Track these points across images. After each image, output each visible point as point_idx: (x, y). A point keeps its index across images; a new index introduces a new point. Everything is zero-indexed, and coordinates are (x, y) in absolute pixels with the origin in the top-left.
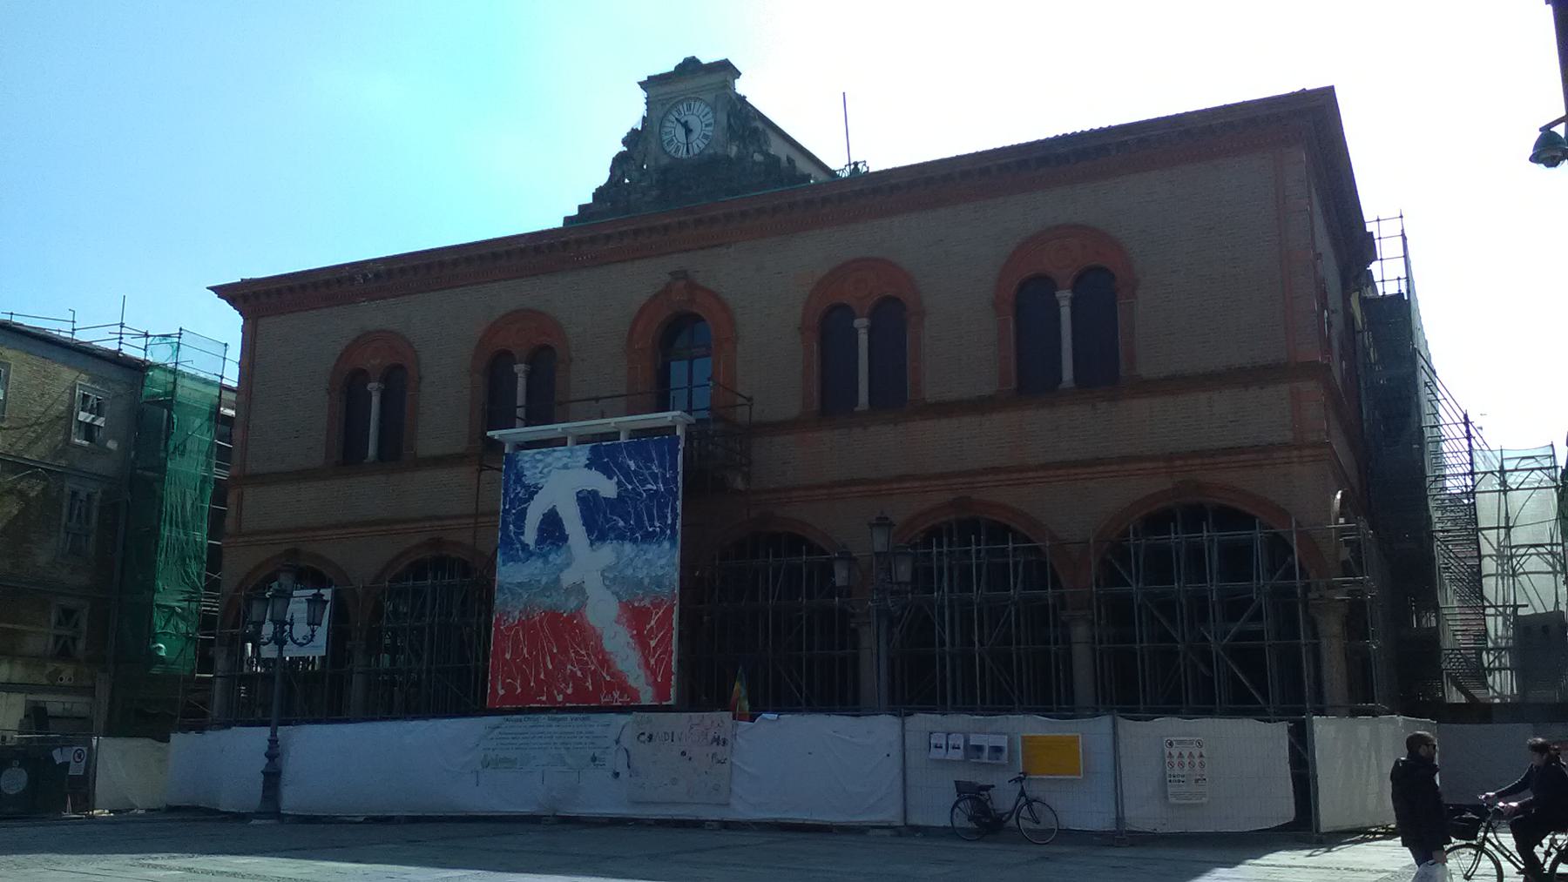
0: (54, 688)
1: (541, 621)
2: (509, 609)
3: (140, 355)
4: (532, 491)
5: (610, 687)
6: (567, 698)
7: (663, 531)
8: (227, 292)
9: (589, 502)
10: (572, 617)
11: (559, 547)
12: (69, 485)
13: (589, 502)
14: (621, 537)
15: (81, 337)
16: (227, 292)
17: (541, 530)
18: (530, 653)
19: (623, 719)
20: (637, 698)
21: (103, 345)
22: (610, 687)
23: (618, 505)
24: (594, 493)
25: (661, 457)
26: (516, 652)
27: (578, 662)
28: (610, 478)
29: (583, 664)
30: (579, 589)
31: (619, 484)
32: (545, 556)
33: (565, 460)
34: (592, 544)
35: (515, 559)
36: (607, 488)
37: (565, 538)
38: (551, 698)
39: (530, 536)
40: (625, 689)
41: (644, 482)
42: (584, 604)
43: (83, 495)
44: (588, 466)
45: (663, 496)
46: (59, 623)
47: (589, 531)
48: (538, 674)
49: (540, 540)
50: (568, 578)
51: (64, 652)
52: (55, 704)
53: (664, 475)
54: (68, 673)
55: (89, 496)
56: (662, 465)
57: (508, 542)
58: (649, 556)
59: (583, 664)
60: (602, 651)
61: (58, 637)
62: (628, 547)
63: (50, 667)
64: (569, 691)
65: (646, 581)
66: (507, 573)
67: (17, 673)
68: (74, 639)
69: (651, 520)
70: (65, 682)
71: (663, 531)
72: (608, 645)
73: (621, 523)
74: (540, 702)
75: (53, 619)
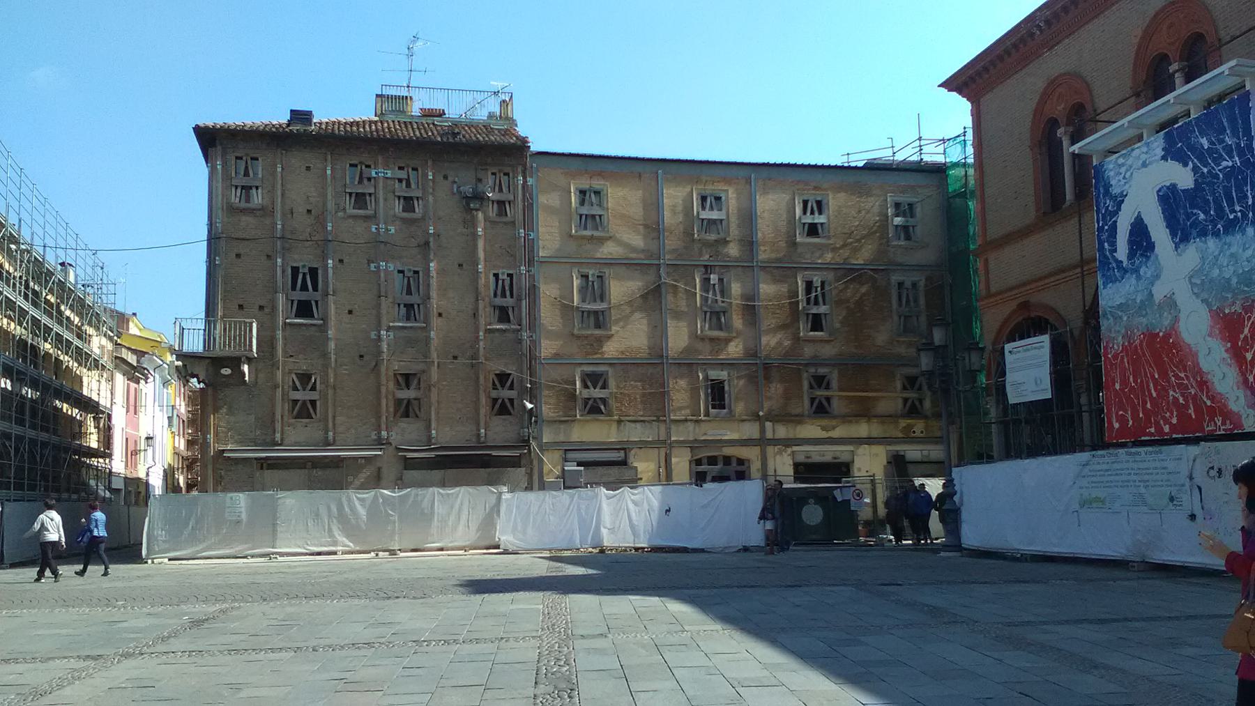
0: (908, 438)
1: (1141, 344)
2: (1114, 334)
3: (940, 159)
4: (1119, 201)
5: (1212, 412)
6: (1173, 428)
7: (1245, 216)
8: (953, 84)
9: (1169, 198)
10: (1168, 336)
11: (1148, 258)
12: (895, 278)
13: (1169, 198)
14: (1203, 234)
15: (900, 157)
16: (953, 84)
17: (1131, 242)
18: (1135, 381)
19: (1193, 450)
20: (1241, 426)
21: (911, 159)
22: (1212, 412)
23: (1194, 196)
24: (1173, 188)
25: (1233, 120)
26: (1125, 382)
27: (1180, 386)
28: (1186, 165)
29: (1183, 388)
30: (1170, 303)
31: (1195, 169)
32: (1136, 271)
33: (1144, 157)
34: (1176, 248)
35: (1110, 280)
36: (1183, 177)
37: (1151, 246)
38: (1160, 430)
39: (1122, 252)
40: (1227, 415)
41: (1217, 161)
42: (1176, 319)
43: (908, 284)
44: (1164, 158)
45: (1240, 171)
46: (905, 388)
47: (1173, 234)
48: (1145, 403)
49: (1131, 255)
50: (1159, 292)
51: (913, 410)
52: (913, 452)
53: (1238, 145)
54: (919, 427)
55: (823, 283)
56: (1235, 134)
57: (1105, 263)
58: (1233, 250)
59: (1183, 388)
60: (1200, 372)
61: (906, 400)
62: (1212, 243)
63: (903, 423)
64: (1174, 421)
65: (1234, 280)
66: (1111, 296)
67: (875, 429)
68: (921, 401)
69: (1231, 204)
70: (918, 434)
71: (1245, 216)
72: (1205, 365)
73: (1202, 216)
74: (1151, 434)
75: (899, 385)
